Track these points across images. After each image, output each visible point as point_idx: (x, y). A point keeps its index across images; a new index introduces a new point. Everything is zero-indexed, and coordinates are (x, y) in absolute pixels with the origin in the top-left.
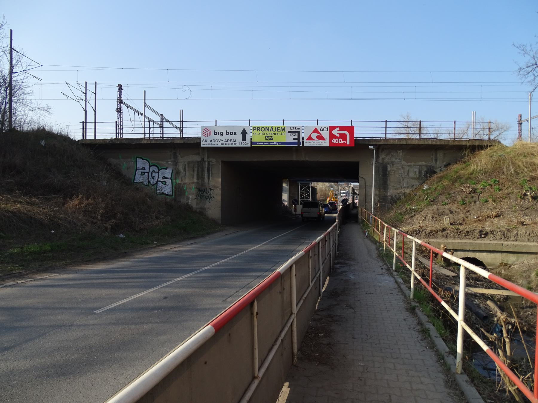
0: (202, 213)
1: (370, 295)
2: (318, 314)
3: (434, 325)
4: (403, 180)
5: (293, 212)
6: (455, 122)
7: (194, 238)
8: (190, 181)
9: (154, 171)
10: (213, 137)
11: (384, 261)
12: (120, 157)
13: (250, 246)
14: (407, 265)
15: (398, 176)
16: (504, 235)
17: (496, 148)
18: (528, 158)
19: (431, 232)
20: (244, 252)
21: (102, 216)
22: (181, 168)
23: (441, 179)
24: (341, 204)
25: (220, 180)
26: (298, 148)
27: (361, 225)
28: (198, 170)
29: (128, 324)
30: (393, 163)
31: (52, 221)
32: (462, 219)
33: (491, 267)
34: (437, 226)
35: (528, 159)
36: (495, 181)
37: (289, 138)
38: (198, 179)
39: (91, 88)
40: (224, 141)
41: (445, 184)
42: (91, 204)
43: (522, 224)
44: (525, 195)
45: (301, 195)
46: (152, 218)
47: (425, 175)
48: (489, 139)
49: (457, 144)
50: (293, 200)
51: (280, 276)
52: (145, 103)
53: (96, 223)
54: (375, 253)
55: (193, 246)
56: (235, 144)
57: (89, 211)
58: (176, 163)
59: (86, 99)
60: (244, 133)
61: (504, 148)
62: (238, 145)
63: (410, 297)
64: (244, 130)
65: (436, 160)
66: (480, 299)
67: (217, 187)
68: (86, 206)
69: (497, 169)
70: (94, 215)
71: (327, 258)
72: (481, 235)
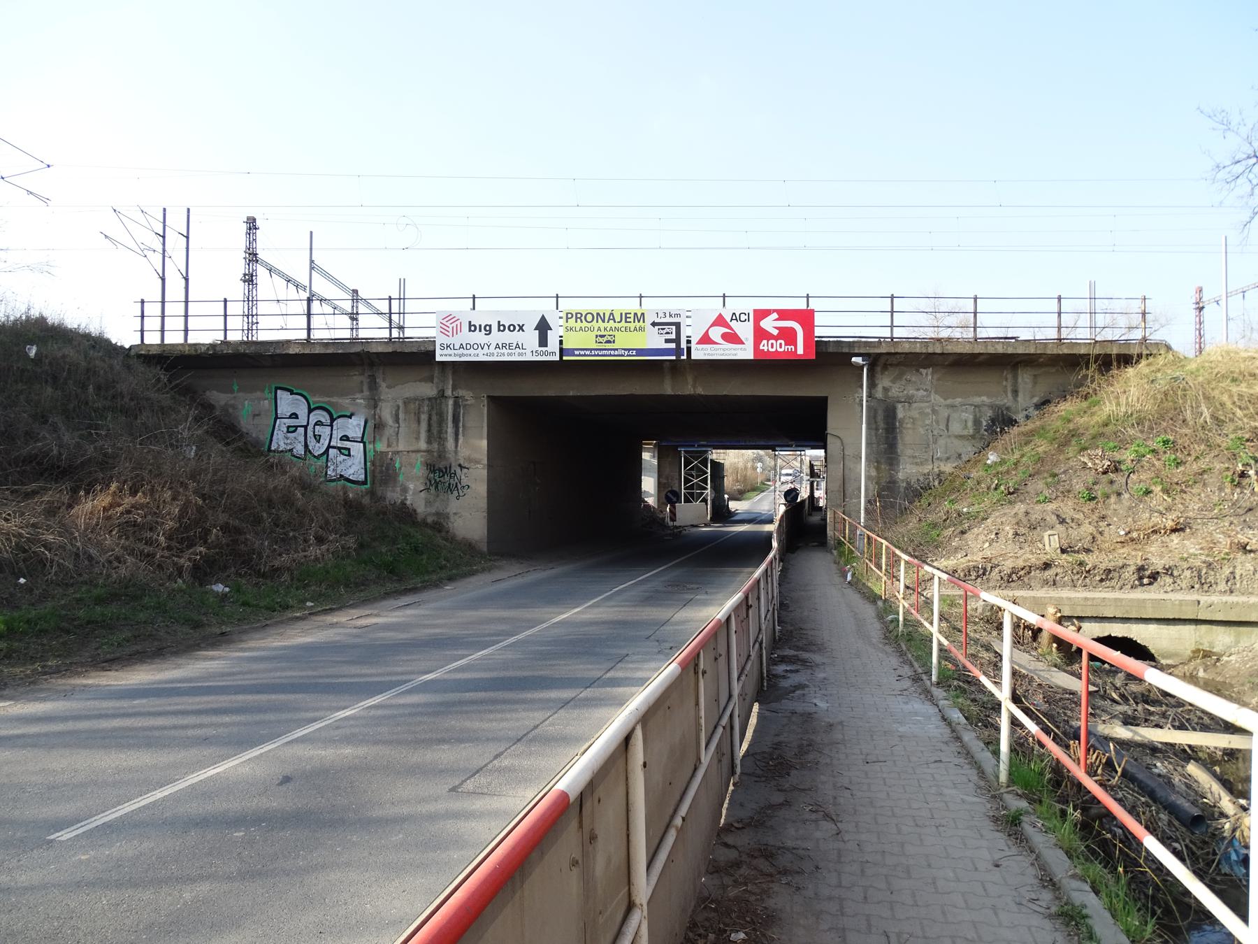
0: (439, 526)
1: (877, 767)
2: (726, 845)
3: (1097, 892)
4: (935, 442)
5: (668, 520)
6: (1059, 298)
7: (414, 590)
8: (408, 447)
9: (319, 423)
10: (466, 337)
11: (902, 654)
12: (236, 388)
13: (557, 610)
14: (984, 680)
15: (922, 431)
16: (1200, 577)
17: (1161, 361)
18: (1244, 385)
19: (1014, 571)
20: (536, 629)
21: (169, 538)
22: (386, 413)
23: (1029, 437)
24: (783, 501)
25: (484, 443)
26: (678, 365)
27: (835, 552)
28: (430, 419)
29: (136, 886)
30: (909, 401)
31: (25, 551)
32: (1090, 538)
33: (1169, 662)
34: (1026, 556)
35: (1243, 388)
36: (1166, 442)
37: (655, 340)
38: (429, 442)
39: (176, 222)
40: (492, 347)
41: (1040, 450)
42: (142, 506)
43: (1244, 548)
44: (1243, 475)
45: (687, 481)
46: (306, 541)
47: (990, 429)
48: (1145, 339)
49: (1066, 351)
50: (669, 495)
51: (567, 813)
52: (312, 261)
53: (153, 555)
54: (875, 629)
55: (409, 612)
56: (520, 354)
57: (135, 524)
58: (374, 403)
59: (164, 251)
60: (543, 327)
61: (1179, 361)
62: (529, 357)
63: (997, 777)
64: (543, 319)
65: (1015, 392)
66: (1166, 758)
67: (478, 462)
68: (128, 512)
69: (1169, 410)
70: (149, 534)
71: (753, 654)
72: (1141, 578)
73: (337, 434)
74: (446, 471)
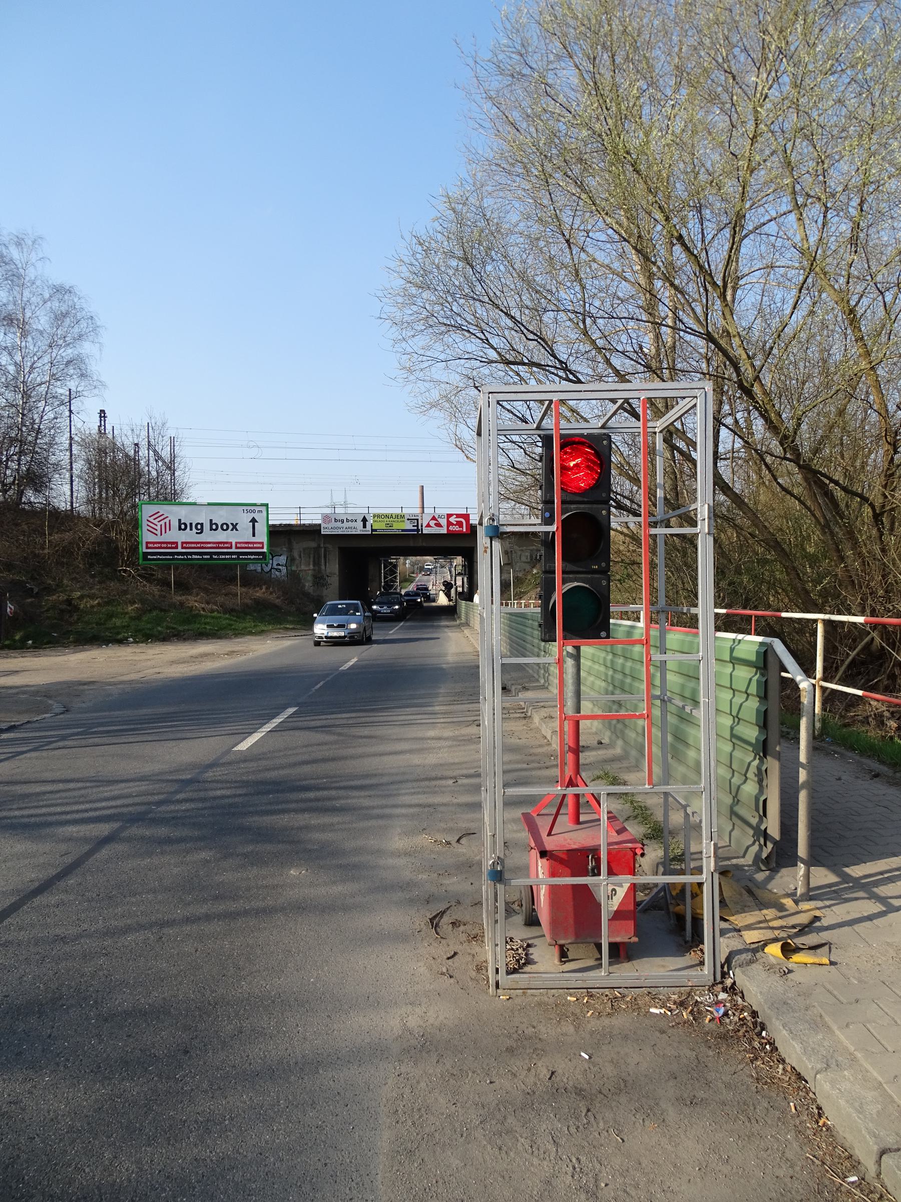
22: (296, 554)
37: (409, 526)
38: (314, 566)
58: (290, 550)
60: (364, 520)
73: (275, 563)
74: (322, 578)
